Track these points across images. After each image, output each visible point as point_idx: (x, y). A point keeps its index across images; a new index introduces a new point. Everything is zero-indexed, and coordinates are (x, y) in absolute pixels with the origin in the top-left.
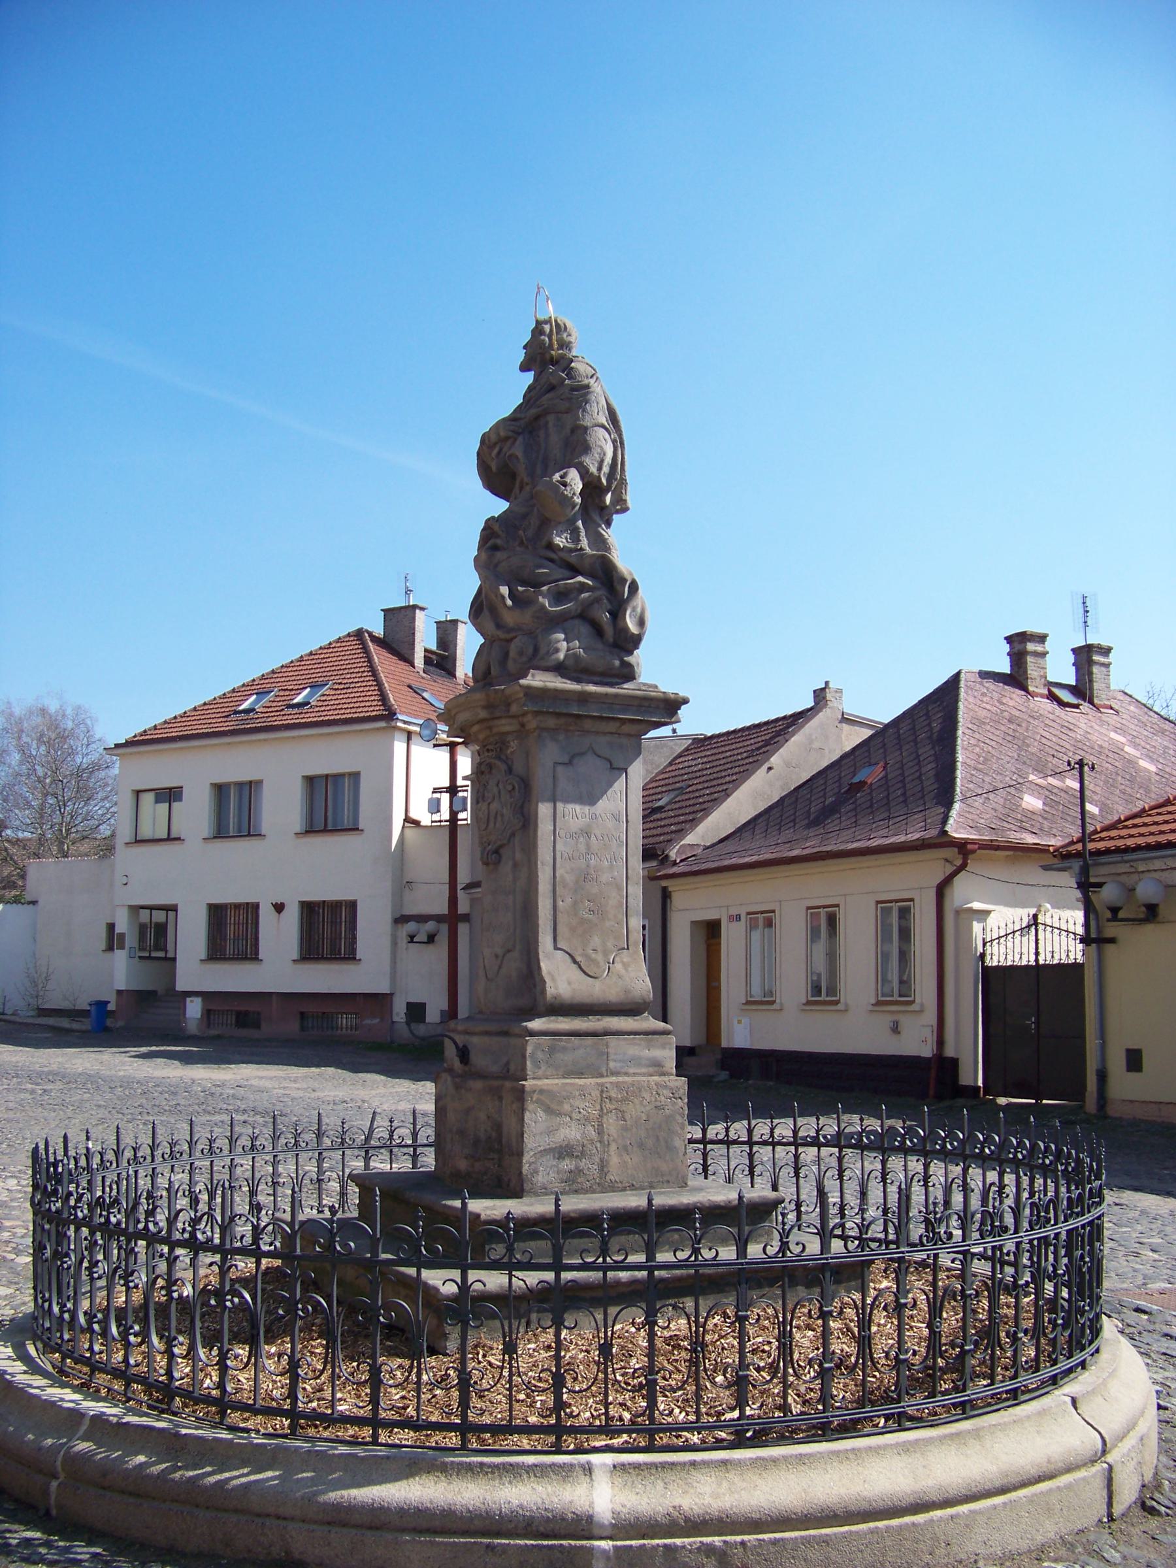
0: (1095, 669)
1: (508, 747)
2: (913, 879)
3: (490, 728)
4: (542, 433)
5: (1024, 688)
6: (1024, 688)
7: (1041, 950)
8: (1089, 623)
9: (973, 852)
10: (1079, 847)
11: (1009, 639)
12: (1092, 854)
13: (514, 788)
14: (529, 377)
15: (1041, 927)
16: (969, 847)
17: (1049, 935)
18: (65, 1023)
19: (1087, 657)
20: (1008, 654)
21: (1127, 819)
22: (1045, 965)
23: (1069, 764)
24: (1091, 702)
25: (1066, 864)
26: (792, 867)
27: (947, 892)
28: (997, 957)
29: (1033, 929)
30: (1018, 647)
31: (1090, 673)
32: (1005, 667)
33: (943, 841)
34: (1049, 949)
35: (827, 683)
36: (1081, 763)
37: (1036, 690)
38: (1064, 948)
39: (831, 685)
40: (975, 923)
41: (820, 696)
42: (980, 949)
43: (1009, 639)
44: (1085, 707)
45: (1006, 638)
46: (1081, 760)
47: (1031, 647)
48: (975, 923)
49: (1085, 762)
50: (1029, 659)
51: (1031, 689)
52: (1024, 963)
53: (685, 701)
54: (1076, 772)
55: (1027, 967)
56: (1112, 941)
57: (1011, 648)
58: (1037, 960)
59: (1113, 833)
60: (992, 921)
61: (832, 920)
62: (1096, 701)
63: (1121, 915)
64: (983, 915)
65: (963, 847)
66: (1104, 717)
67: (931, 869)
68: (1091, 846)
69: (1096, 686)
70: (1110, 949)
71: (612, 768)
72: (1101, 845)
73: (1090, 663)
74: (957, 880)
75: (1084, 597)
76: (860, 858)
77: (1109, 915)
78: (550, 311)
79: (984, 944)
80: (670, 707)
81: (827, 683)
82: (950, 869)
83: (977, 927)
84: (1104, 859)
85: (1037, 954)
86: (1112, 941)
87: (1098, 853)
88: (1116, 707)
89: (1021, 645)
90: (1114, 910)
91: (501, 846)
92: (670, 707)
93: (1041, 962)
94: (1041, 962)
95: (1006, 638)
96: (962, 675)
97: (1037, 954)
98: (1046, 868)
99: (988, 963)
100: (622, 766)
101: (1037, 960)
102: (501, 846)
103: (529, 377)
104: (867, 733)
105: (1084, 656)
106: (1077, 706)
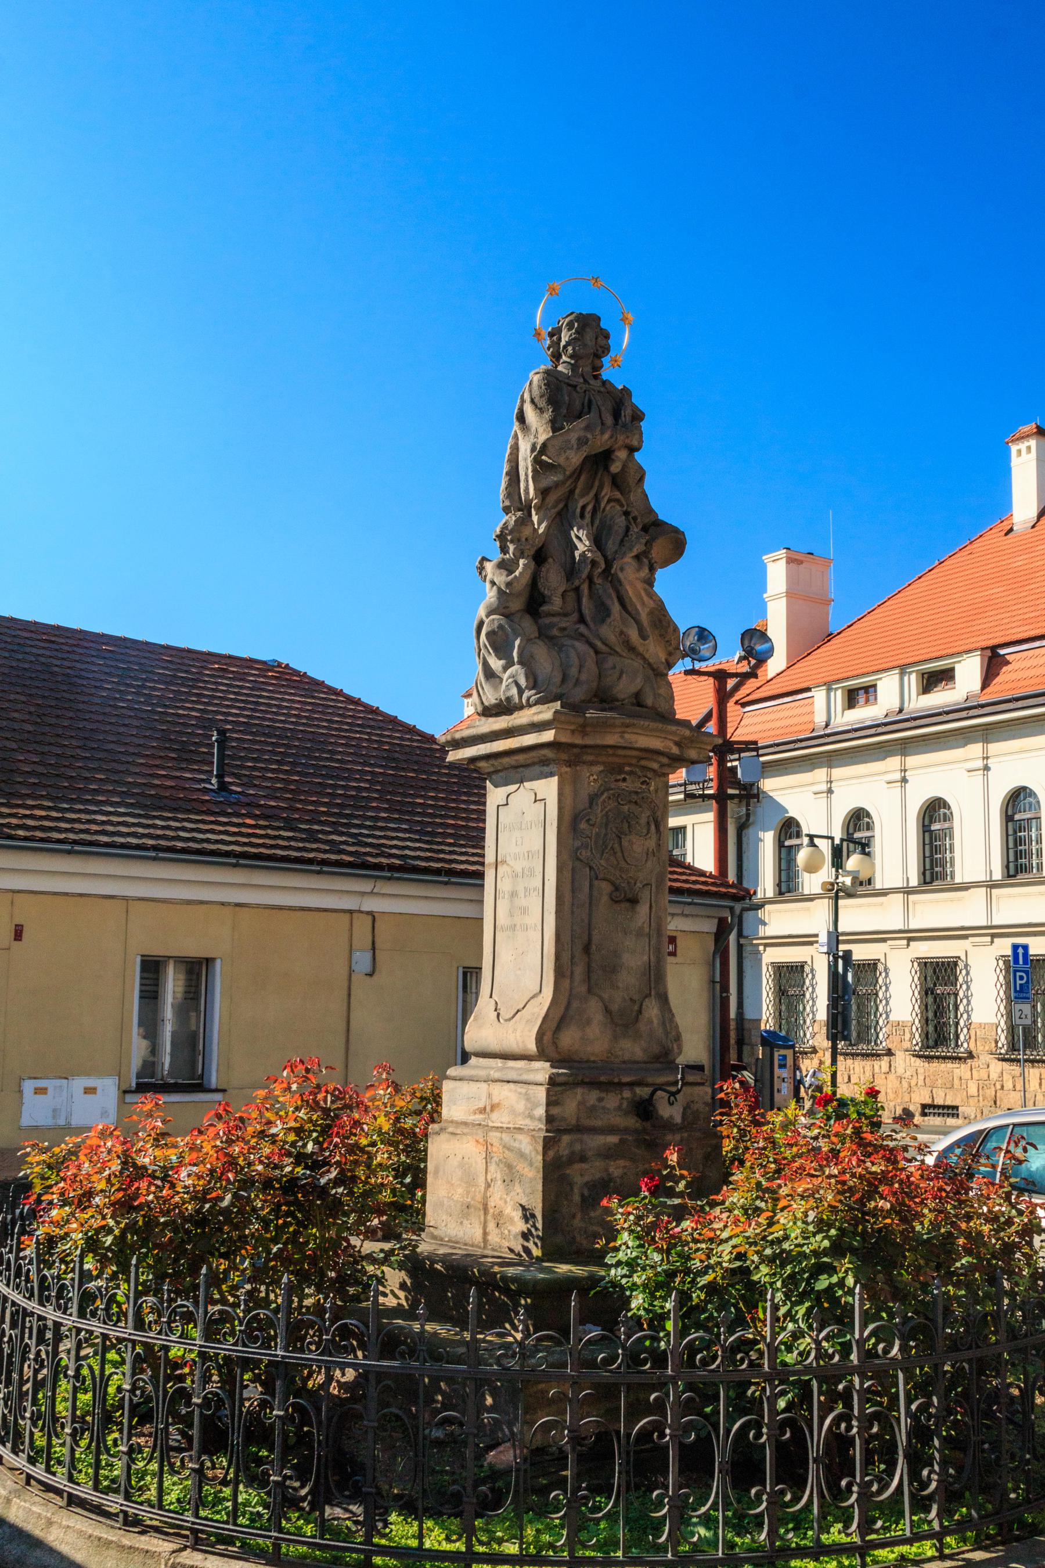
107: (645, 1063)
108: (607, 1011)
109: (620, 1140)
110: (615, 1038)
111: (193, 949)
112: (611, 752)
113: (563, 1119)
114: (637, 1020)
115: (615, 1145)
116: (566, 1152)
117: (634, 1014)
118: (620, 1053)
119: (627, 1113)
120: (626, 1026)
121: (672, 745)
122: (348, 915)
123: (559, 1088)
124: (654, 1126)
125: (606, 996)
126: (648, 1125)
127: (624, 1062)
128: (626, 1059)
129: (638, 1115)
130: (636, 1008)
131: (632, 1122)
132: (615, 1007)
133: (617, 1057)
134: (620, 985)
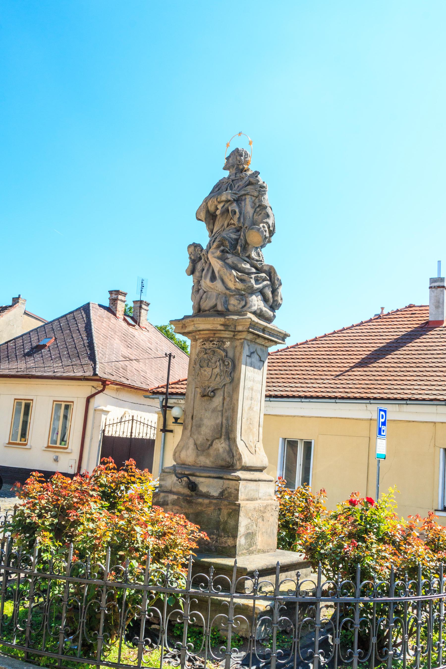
0: (142, 311)
1: (224, 345)
2: (76, 393)
3: (214, 334)
4: (243, 203)
5: (115, 314)
6: (115, 314)
7: (134, 431)
8: (143, 291)
9: (108, 385)
10: (164, 390)
11: (111, 292)
12: (170, 394)
13: (229, 364)
14: (226, 174)
15: (135, 421)
16: (107, 382)
17: (138, 425)
18: (211, 469)
19: (139, 304)
20: (109, 299)
21: (182, 381)
22: (135, 439)
23: (166, 354)
24: (139, 325)
25: (155, 396)
26: (32, 380)
27: (92, 400)
28: (110, 432)
29: (131, 422)
30: (114, 296)
31: (140, 313)
32: (107, 304)
33: (95, 378)
34: (137, 431)
35: (19, 295)
36: (170, 355)
37: (119, 316)
38: (145, 431)
39: (21, 297)
40: (103, 415)
41: (16, 300)
42: (104, 428)
43: (111, 292)
44: (137, 326)
45: (109, 292)
46: (170, 354)
47: (120, 297)
48: (103, 415)
49: (172, 354)
50: (119, 302)
51: (117, 315)
52: (125, 436)
53: (289, 336)
54: (168, 358)
55: (126, 438)
56: (171, 431)
57: (111, 296)
58: (131, 435)
59: (178, 386)
60: (109, 416)
61: (27, 407)
62: (141, 325)
63: (179, 421)
64: (107, 412)
65: (104, 382)
66: (144, 332)
67: (86, 389)
68: (170, 390)
69: (142, 318)
70: (169, 435)
71: (261, 360)
72: (173, 391)
73: (141, 307)
74: (97, 396)
75: (143, 280)
76: (51, 380)
77: (174, 421)
78: (242, 145)
79: (105, 426)
80: (284, 337)
81: (19, 295)
82: (94, 391)
83: (103, 417)
84: (174, 397)
85: (131, 433)
86: (171, 431)
87: (172, 394)
88: (148, 329)
89: (115, 295)
90: (176, 419)
91: (217, 389)
92: (284, 337)
93: (133, 437)
94: (133, 437)
95: (109, 292)
96: (91, 304)
97: (131, 433)
98: (146, 397)
99: (106, 434)
100: (263, 360)
101: (131, 435)
102: (217, 389)
103: (226, 174)
104: (41, 324)
105: (138, 305)
106: (134, 326)
107: (212, 468)
108: (195, 444)
109: (178, 497)
110: (197, 456)
111: (307, 438)
112: (198, 333)
113: (166, 487)
114: (209, 448)
115: (176, 499)
116: (162, 500)
117: (208, 446)
118: (199, 462)
119: (184, 487)
120: (203, 451)
121: (218, 326)
122: (433, 424)
123: (165, 474)
124: (196, 494)
125: (195, 437)
126: (193, 493)
127: (201, 466)
128: (202, 465)
129: (189, 488)
130: (209, 443)
131: (186, 491)
132: (198, 442)
133: (198, 464)
134: (202, 433)
